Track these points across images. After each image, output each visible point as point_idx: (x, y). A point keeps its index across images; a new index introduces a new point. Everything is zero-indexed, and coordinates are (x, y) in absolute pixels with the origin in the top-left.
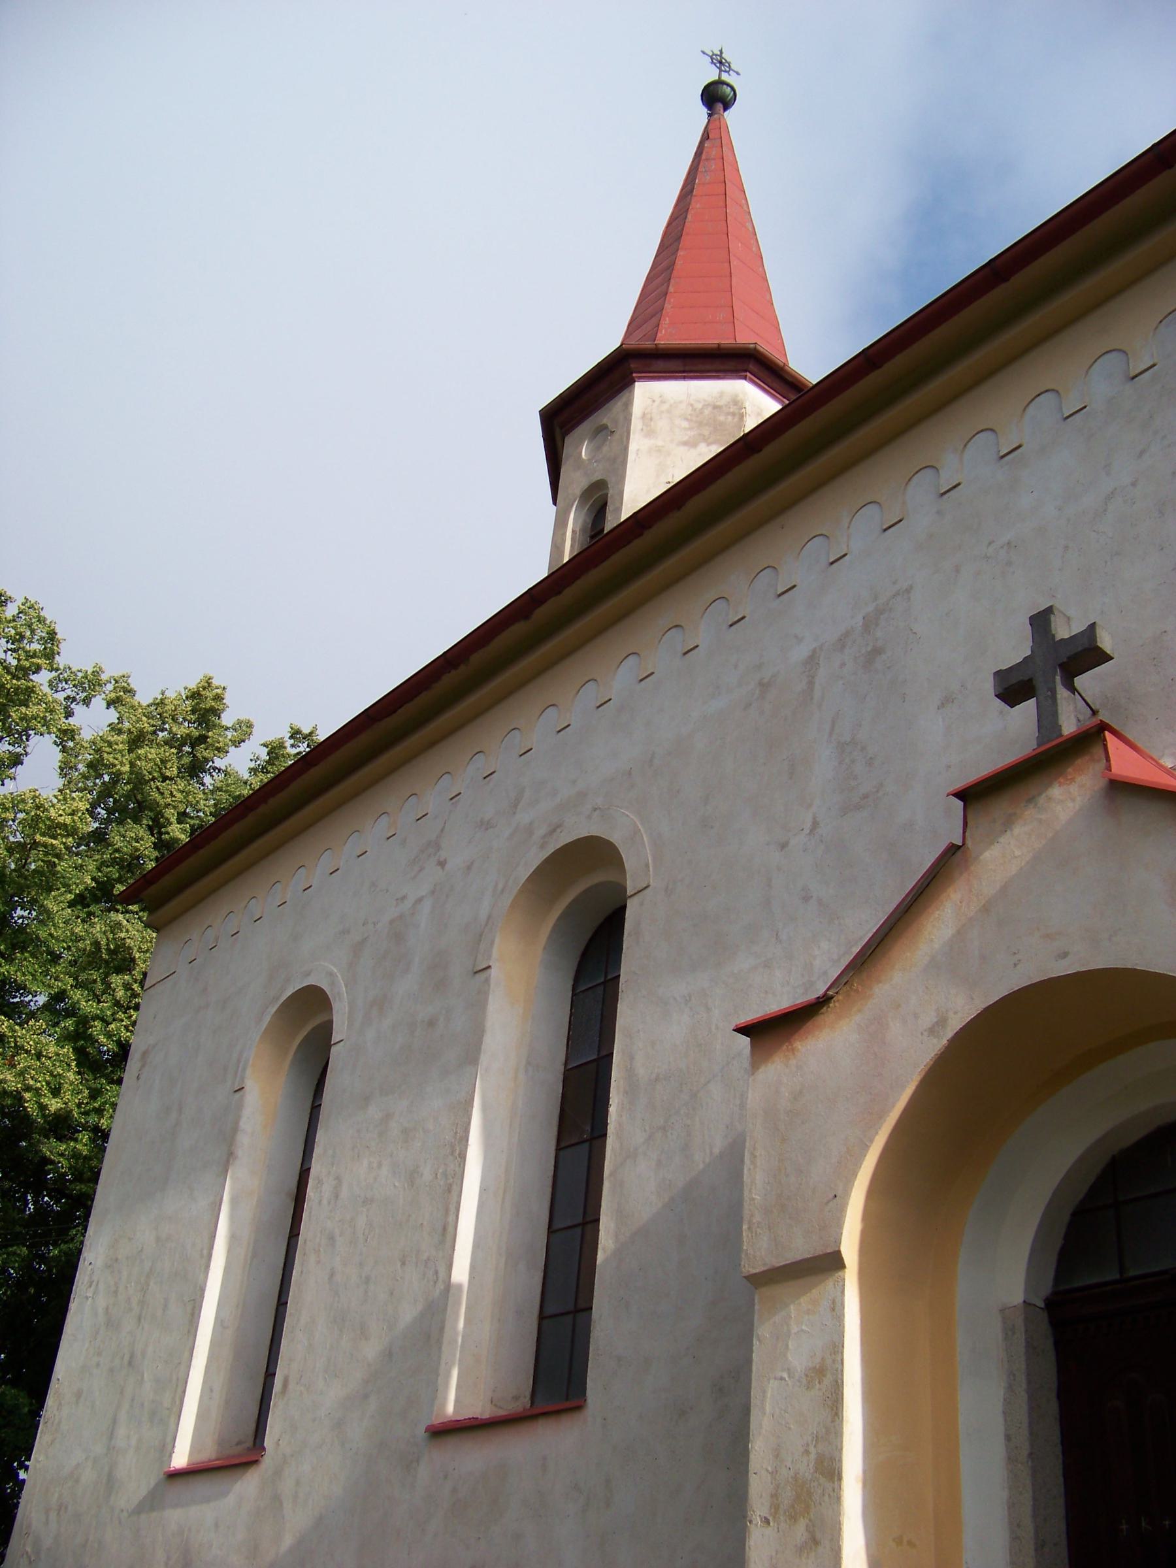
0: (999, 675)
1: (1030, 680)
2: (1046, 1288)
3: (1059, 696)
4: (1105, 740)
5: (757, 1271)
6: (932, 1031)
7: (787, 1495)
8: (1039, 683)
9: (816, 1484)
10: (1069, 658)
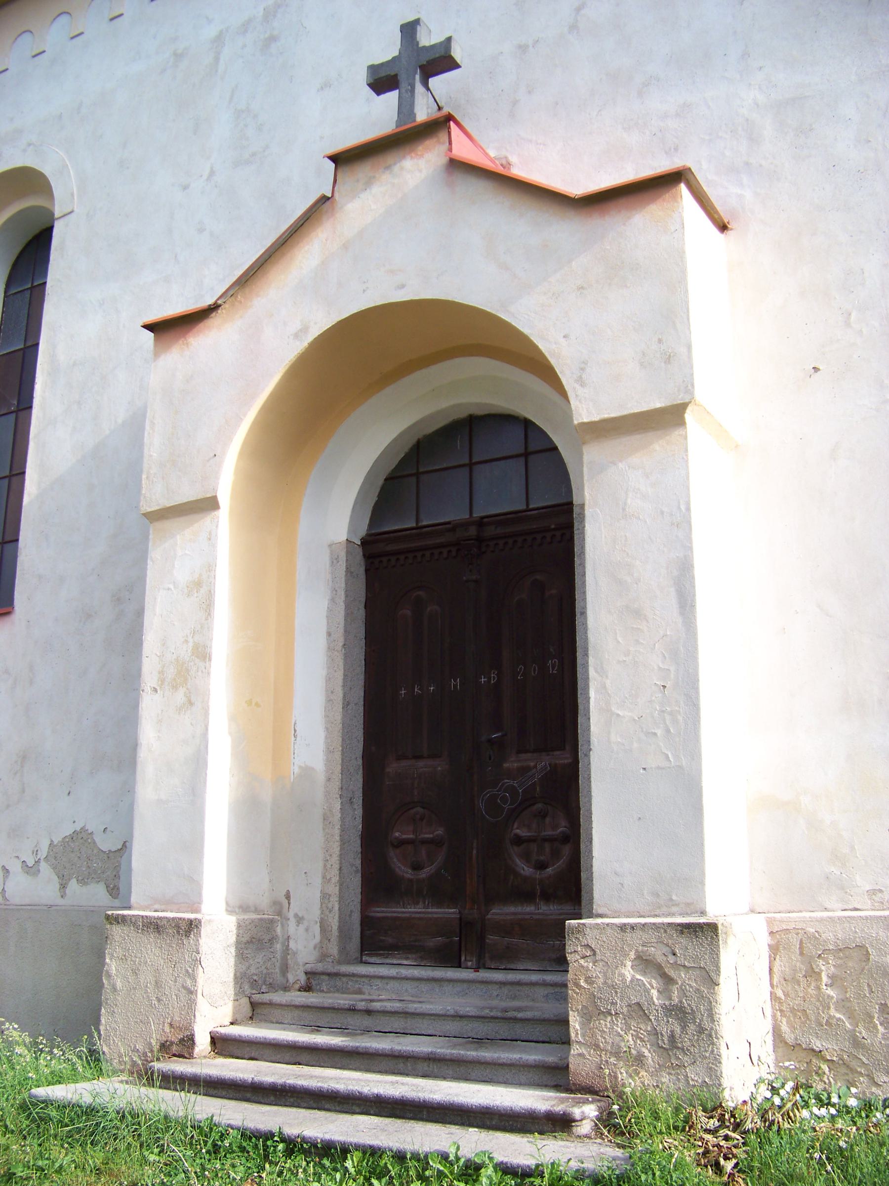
0: (372, 69)
1: (396, 75)
2: (363, 531)
3: (416, 91)
4: (449, 128)
5: (153, 509)
6: (296, 336)
7: (171, 672)
8: (402, 78)
9: (192, 664)
10: (428, 62)
